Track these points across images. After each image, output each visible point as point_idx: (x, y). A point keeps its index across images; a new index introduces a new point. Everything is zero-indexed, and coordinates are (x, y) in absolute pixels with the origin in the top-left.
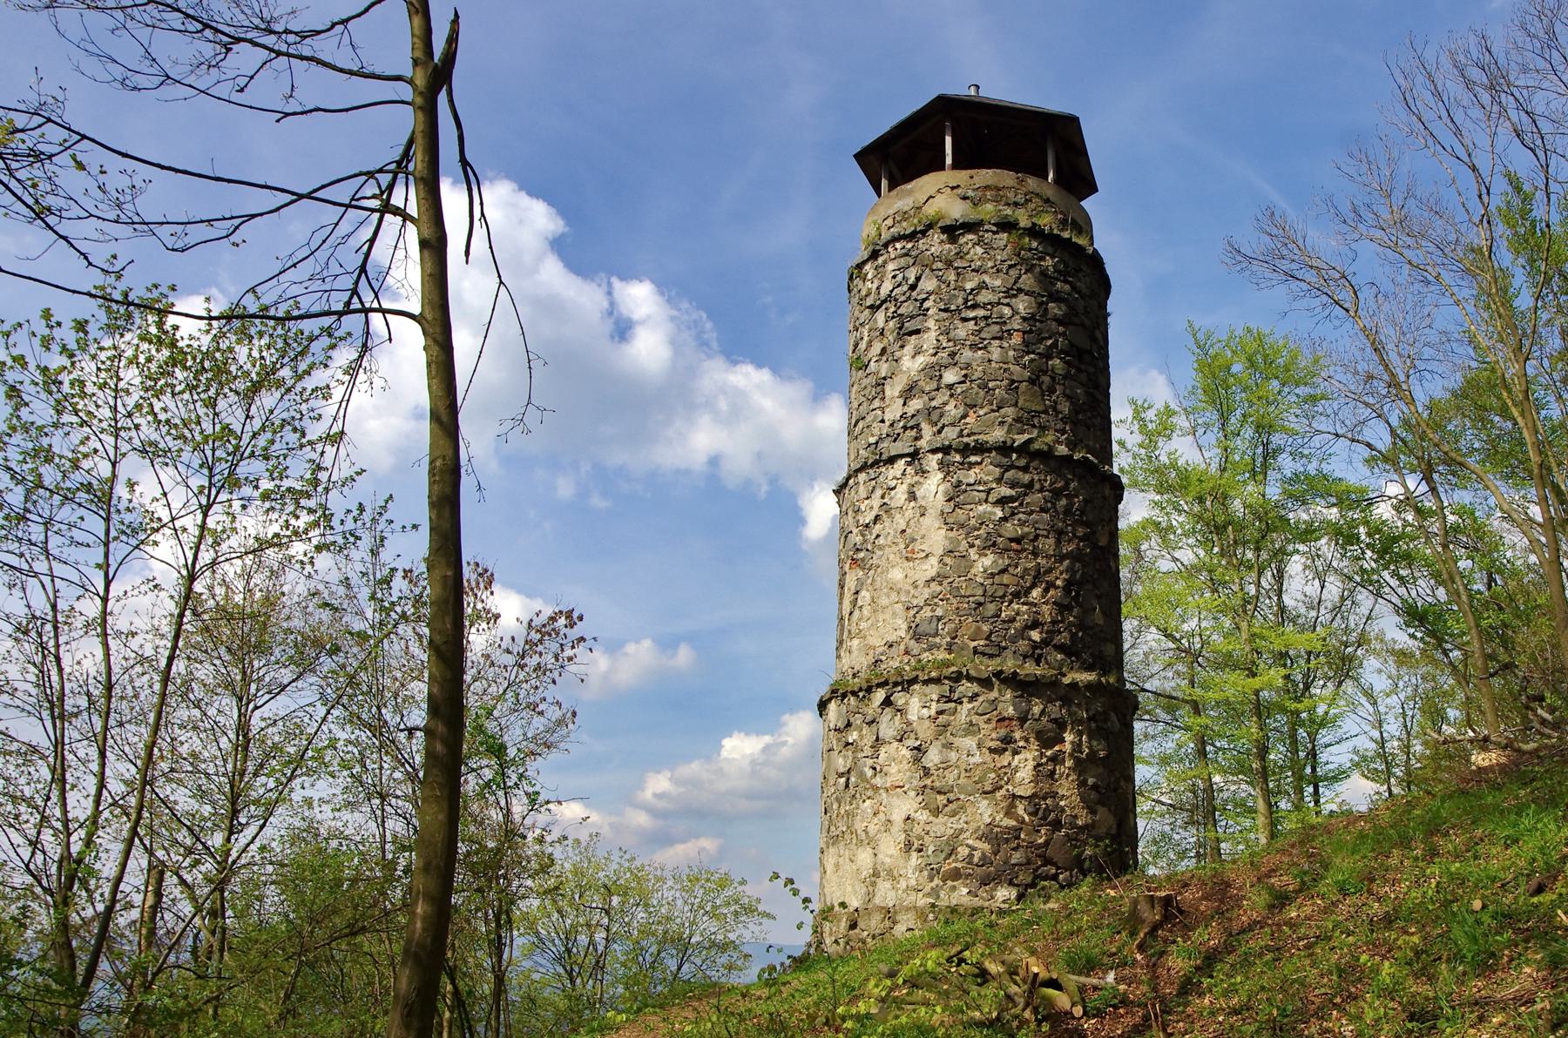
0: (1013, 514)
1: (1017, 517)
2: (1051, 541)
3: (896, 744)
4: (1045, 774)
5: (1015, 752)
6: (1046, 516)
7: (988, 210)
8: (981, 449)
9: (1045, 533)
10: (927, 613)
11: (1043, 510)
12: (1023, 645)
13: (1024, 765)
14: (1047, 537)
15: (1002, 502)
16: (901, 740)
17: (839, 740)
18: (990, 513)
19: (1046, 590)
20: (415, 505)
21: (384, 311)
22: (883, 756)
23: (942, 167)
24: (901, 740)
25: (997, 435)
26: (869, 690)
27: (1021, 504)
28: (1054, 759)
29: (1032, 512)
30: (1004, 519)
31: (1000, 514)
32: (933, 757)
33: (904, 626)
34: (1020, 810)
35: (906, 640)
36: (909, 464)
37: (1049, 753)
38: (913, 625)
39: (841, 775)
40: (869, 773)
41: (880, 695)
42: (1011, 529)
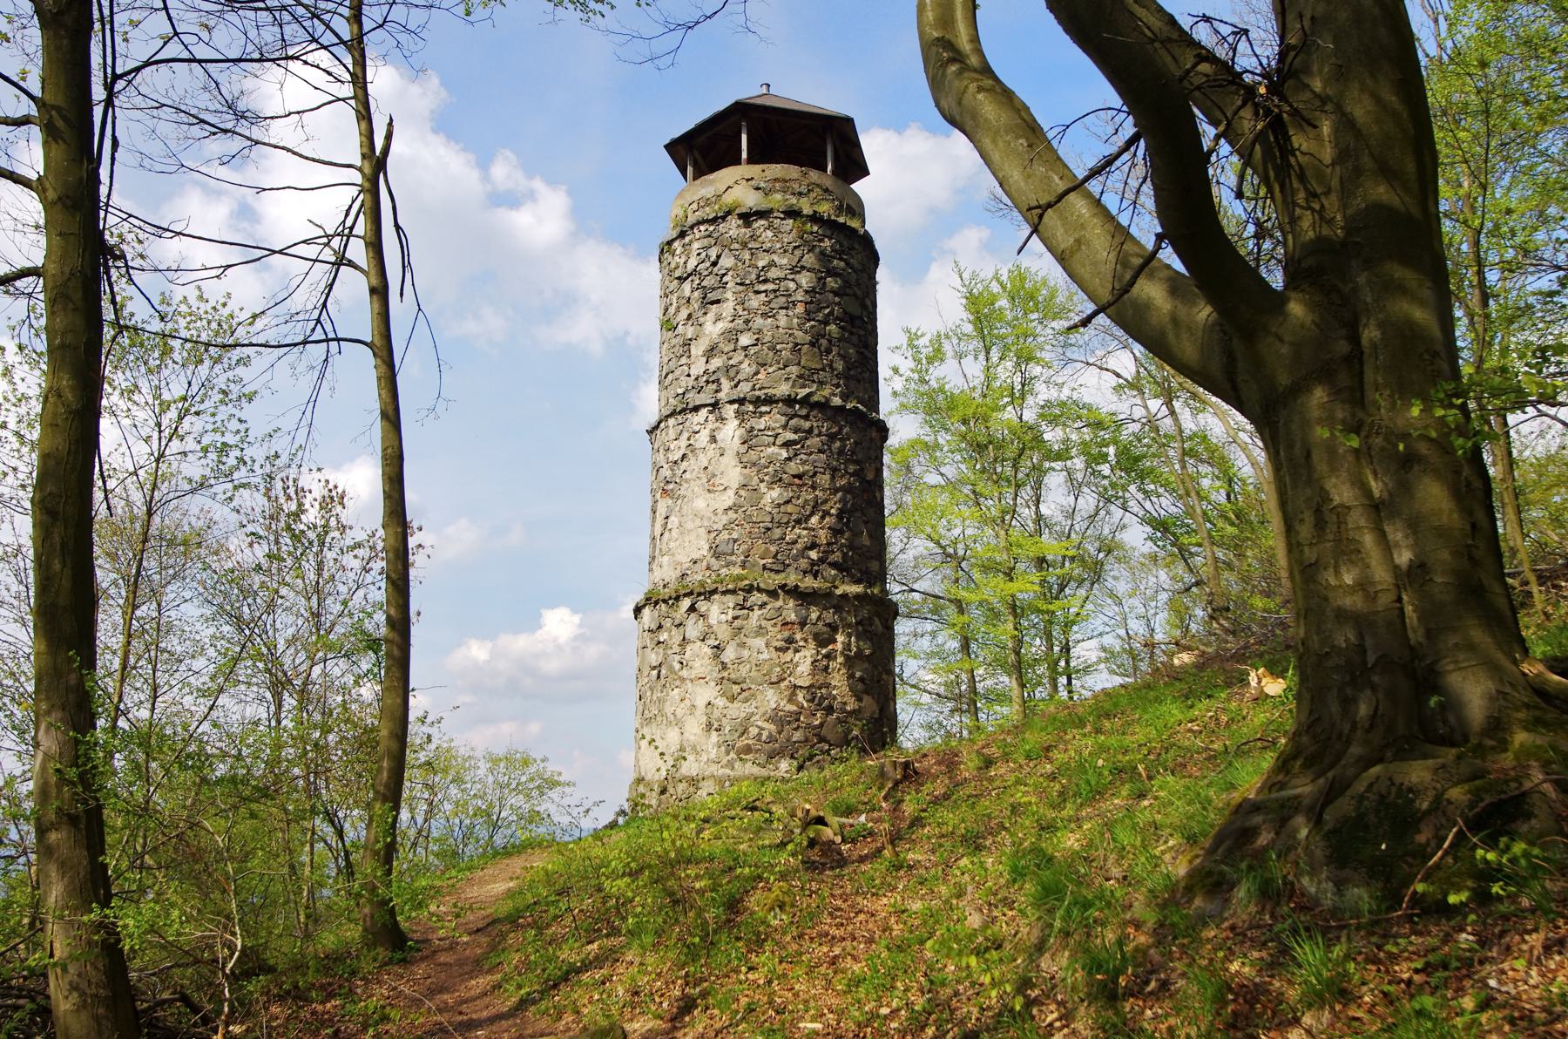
0: (796, 455)
3: (699, 643)
4: (820, 668)
5: (797, 651)
8: (769, 401)
10: (725, 536)
13: (804, 661)
15: (787, 444)
17: (652, 639)
19: (823, 518)
25: (783, 389)
26: (677, 598)
28: (828, 656)
29: (811, 453)
30: (789, 459)
31: (785, 455)
32: (729, 654)
34: (800, 697)
36: (711, 412)
37: (824, 651)
39: (654, 668)
40: (677, 666)
41: (686, 603)
42: (794, 467)
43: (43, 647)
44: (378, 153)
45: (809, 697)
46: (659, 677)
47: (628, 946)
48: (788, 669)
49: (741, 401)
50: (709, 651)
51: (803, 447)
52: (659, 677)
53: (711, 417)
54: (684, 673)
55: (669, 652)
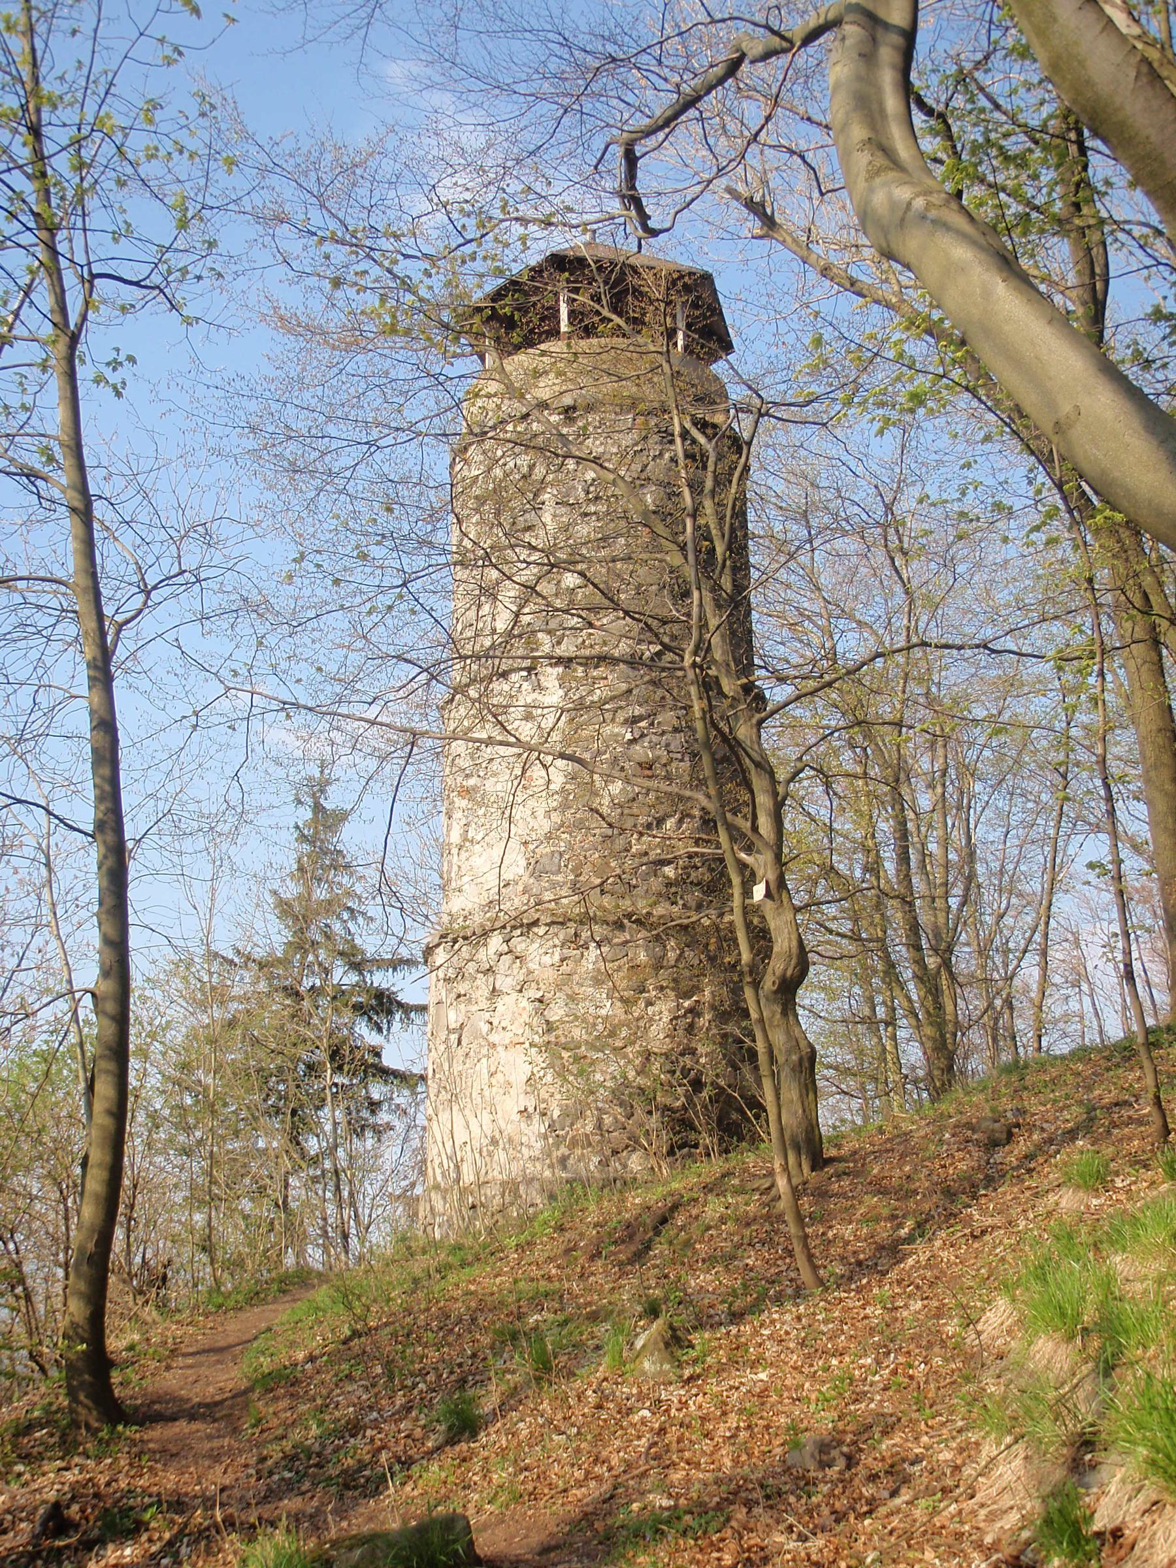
0: (643, 736)
1: (647, 739)
2: (686, 765)
3: (515, 995)
4: (687, 1021)
5: (650, 1003)
6: (680, 737)
7: (608, 386)
8: (602, 659)
9: (679, 756)
10: (545, 849)
11: (676, 730)
12: (656, 884)
13: (663, 1010)
14: (682, 760)
15: (633, 721)
16: (521, 991)
17: (449, 991)
18: (617, 735)
19: (680, 821)
20: (84, 388)
21: (64, 149)
22: (500, 1008)
23: (554, 333)
24: (521, 991)
25: (623, 648)
26: (485, 934)
27: (652, 724)
28: (693, 1011)
29: (663, 733)
30: (633, 741)
31: (629, 736)
32: (556, 1013)
33: (523, 863)
34: (655, 1067)
35: (525, 878)
36: (526, 679)
37: (687, 1004)
38: (532, 861)
39: (454, 1031)
40: (485, 1028)
41: (496, 942)
42: (641, 751)
43: (105, 884)
44: (72, 327)
45: (668, 1067)
46: (459, 1043)
47: (606, 1061)
48: (639, 1029)
49: (566, 662)
50: (530, 1007)
51: (652, 724)
52: (459, 1043)
53: (526, 685)
54: (494, 1038)
55: (474, 1008)
